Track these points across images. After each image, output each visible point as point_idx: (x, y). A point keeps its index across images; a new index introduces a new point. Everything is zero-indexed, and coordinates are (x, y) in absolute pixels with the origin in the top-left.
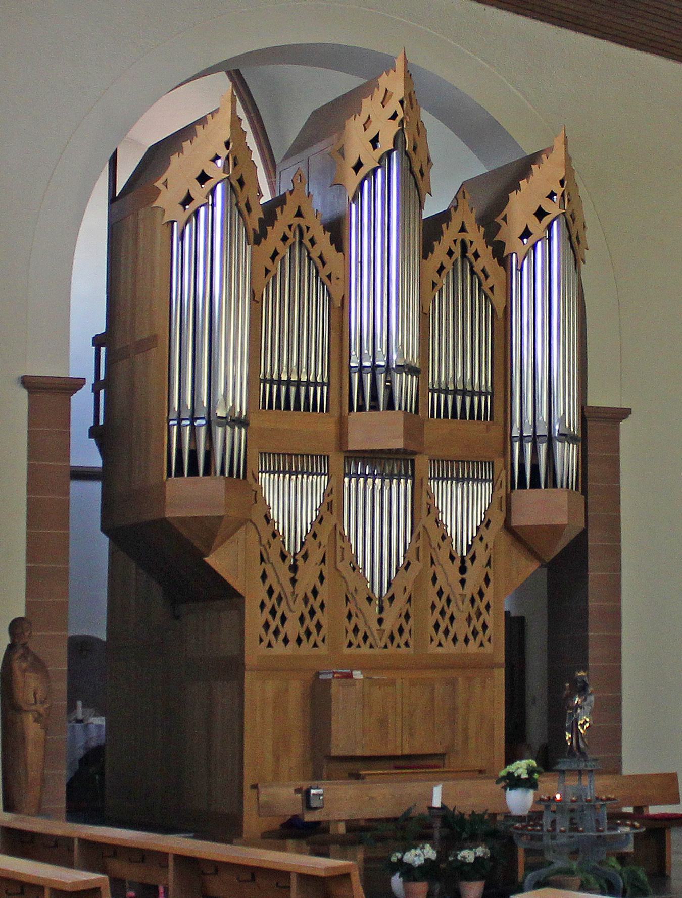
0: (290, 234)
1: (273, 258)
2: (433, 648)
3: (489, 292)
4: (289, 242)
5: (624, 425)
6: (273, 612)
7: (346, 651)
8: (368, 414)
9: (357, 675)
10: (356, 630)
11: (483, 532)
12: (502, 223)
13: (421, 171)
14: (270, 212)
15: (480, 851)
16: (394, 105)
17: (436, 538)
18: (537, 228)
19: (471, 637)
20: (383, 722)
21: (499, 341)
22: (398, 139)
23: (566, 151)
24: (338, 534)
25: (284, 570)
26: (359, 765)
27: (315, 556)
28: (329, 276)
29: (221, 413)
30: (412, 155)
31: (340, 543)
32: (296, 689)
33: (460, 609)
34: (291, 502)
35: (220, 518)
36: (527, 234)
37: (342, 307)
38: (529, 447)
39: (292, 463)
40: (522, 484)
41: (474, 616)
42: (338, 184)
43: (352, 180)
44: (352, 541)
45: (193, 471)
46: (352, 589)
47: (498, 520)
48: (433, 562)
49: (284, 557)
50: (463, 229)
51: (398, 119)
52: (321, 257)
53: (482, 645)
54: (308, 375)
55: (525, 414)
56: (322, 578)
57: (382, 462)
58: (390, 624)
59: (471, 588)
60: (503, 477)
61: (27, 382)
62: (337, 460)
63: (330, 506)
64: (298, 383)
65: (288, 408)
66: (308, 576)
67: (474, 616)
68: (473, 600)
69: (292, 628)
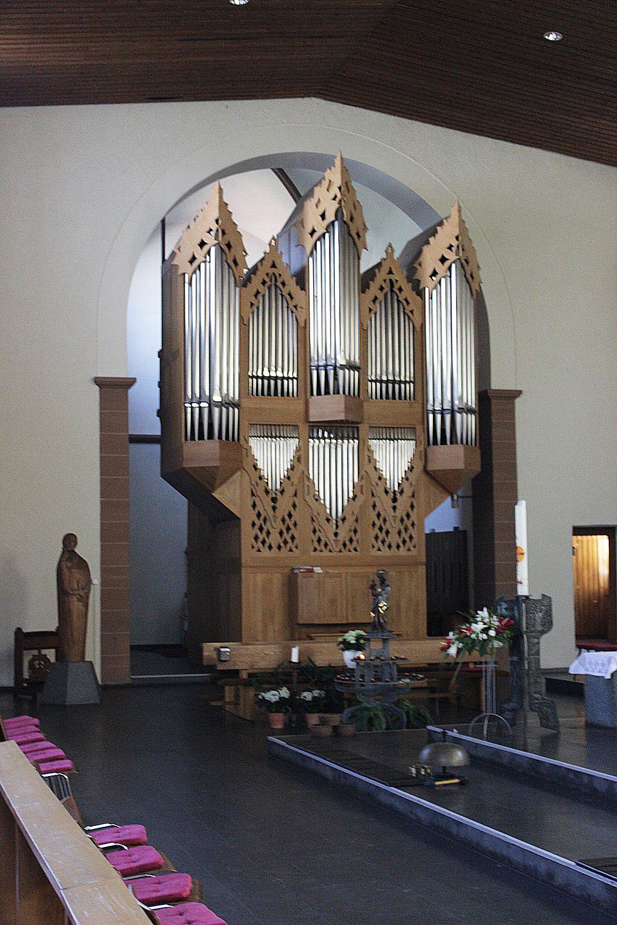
0: (267, 279)
1: (374, 301)
2: (374, 552)
3: (410, 314)
4: (267, 285)
5: (518, 401)
6: (261, 529)
7: (313, 553)
8: (323, 397)
9: (318, 570)
10: (319, 541)
11: (409, 475)
12: (418, 267)
13: (358, 234)
14: (371, 274)
15: (316, 693)
16: (335, 191)
17: (375, 479)
18: (441, 269)
19: (401, 545)
20: (333, 602)
21: (418, 348)
22: (338, 213)
23: (460, 216)
24: (305, 476)
25: (387, 501)
26: (312, 630)
27: (290, 491)
28: (296, 307)
29: (217, 398)
30: (350, 223)
31: (306, 482)
32: (277, 579)
33: (393, 526)
34: (272, 457)
35: (216, 467)
36: (435, 273)
37: (305, 327)
38: (439, 417)
39: (273, 430)
40: (435, 443)
41: (285, 531)
42: (300, 245)
43: (309, 242)
44: (316, 482)
45: (201, 437)
46: (315, 513)
47: (419, 466)
48: (373, 495)
49: (386, 492)
50: (390, 272)
51: (338, 199)
52: (290, 294)
53: (409, 550)
54: (394, 376)
55: (437, 397)
56: (294, 506)
57: (340, 429)
58: (343, 535)
59: (400, 512)
60: (422, 438)
61: (99, 382)
62: (304, 429)
63: (299, 459)
64: (394, 382)
65: (269, 394)
66: (284, 505)
67: (285, 531)
68: (402, 520)
69: (274, 539)
